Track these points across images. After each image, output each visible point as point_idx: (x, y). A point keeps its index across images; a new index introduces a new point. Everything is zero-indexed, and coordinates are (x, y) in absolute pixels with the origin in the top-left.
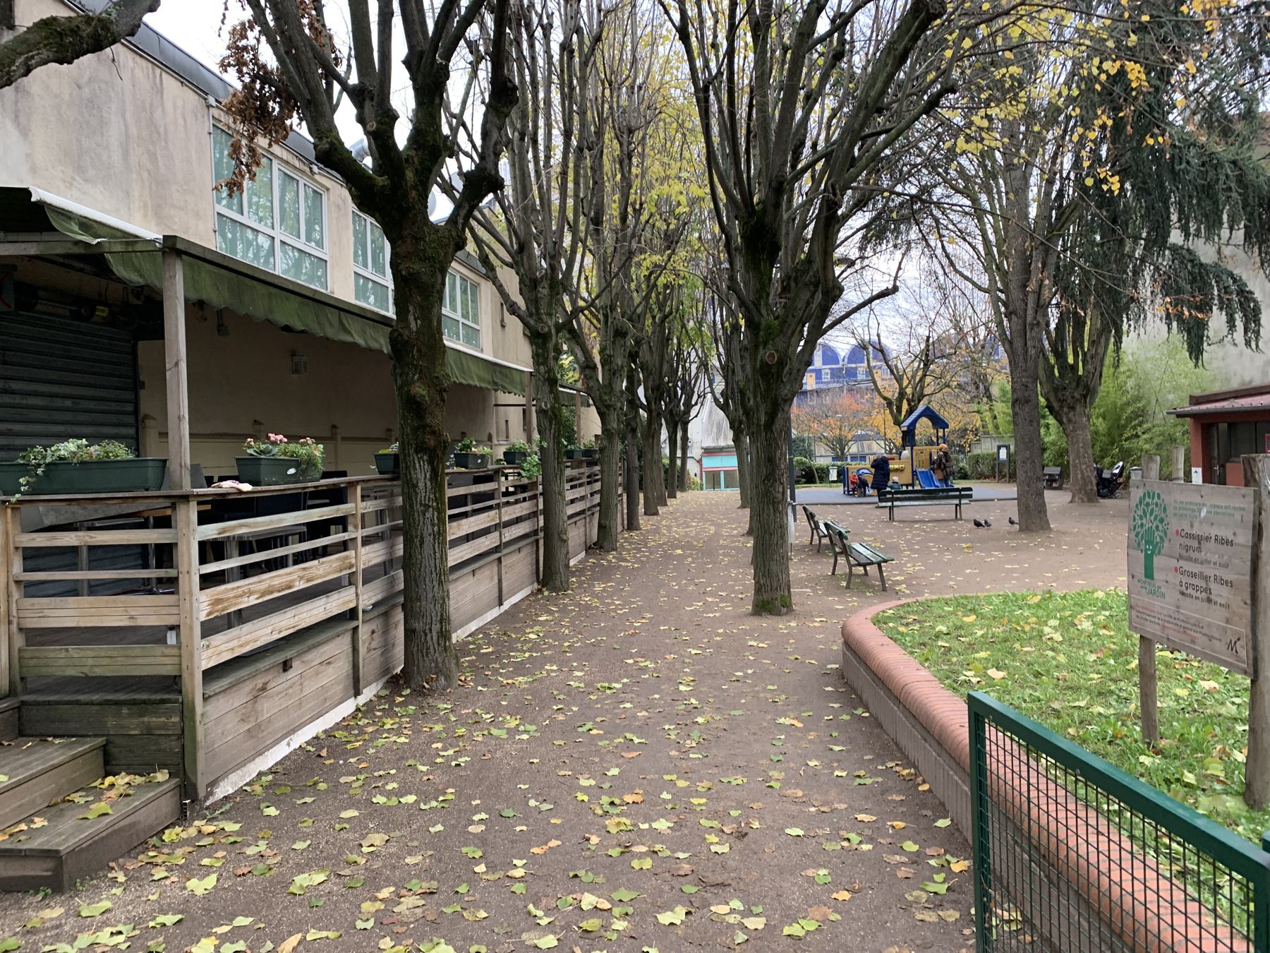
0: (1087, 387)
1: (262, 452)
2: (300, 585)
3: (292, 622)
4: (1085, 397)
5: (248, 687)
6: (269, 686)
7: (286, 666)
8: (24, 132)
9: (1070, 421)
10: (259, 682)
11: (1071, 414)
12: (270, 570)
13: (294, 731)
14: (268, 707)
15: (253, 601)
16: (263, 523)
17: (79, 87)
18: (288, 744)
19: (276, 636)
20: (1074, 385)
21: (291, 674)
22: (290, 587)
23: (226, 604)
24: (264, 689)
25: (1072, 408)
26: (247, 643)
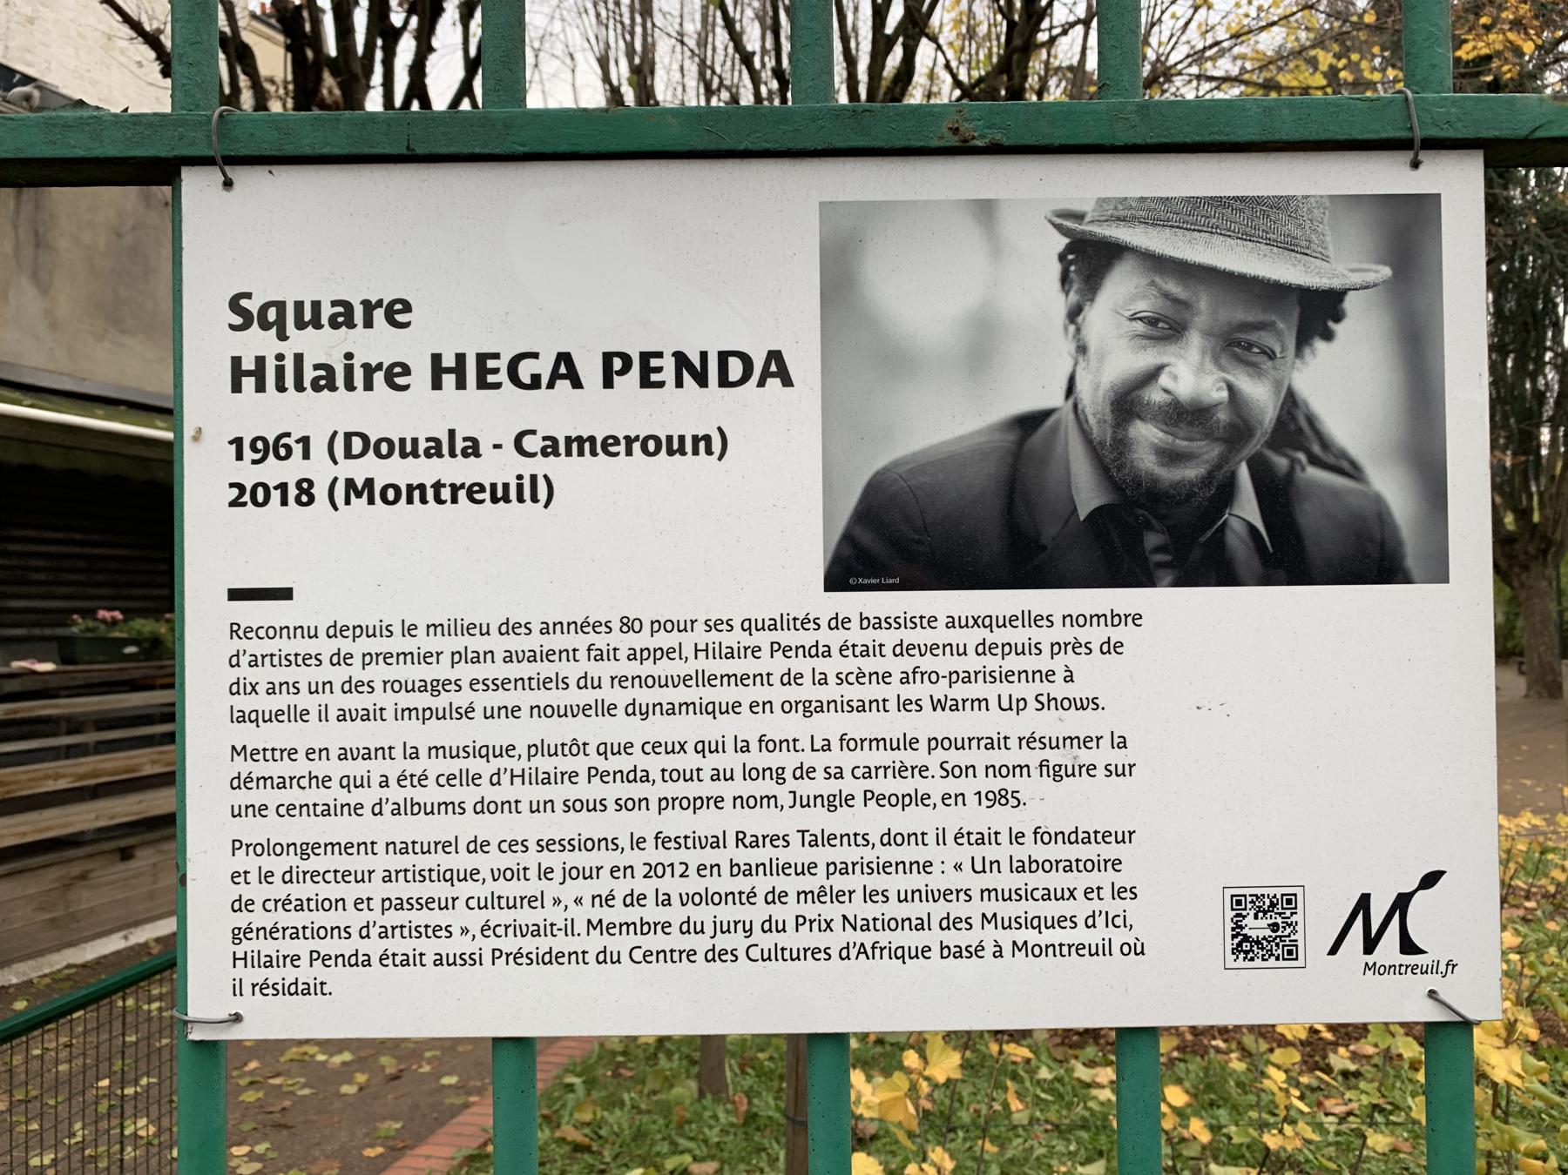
0: (1544, 538)
1: (88, 630)
2: (149, 770)
3: (136, 808)
4: (1545, 552)
5: (55, 873)
6: (91, 875)
7: (126, 854)
8: (44, 289)
9: (1523, 585)
10: (76, 869)
11: (1524, 576)
12: (67, 757)
13: (137, 924)
14: (85, 898)
15: (62, 784)
16: (84, 705)
17: (119, 235)
18: (126, 938)
19: (102, 823)
20: (1527, 537)
21: (132, 864)
22: (135, 771)
23: (13, 787)
24: (83, 876)
25: (1526, 568)
26: (49, 829)
